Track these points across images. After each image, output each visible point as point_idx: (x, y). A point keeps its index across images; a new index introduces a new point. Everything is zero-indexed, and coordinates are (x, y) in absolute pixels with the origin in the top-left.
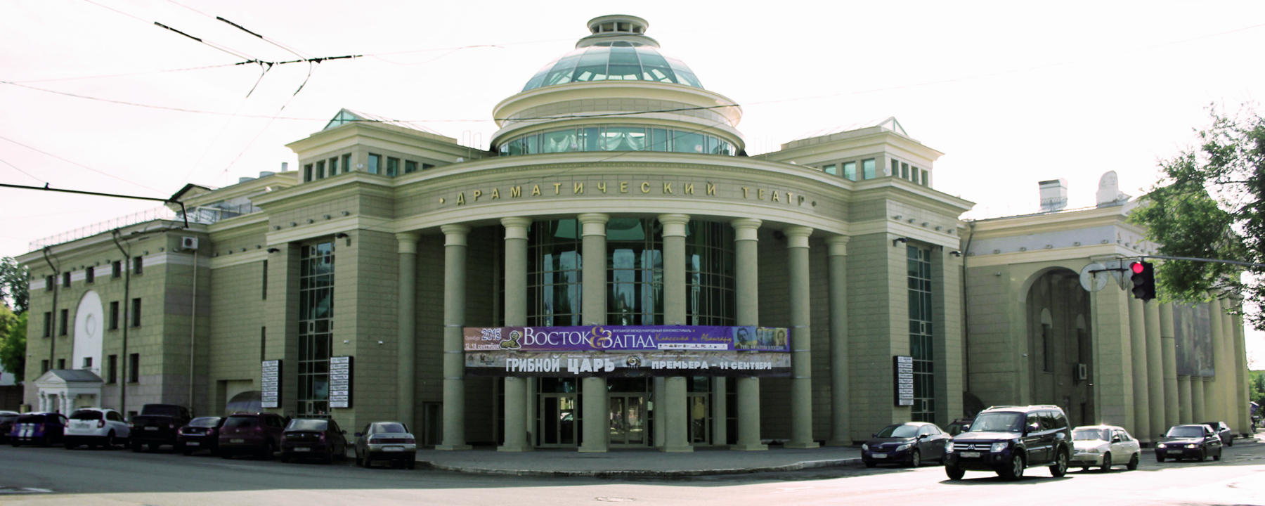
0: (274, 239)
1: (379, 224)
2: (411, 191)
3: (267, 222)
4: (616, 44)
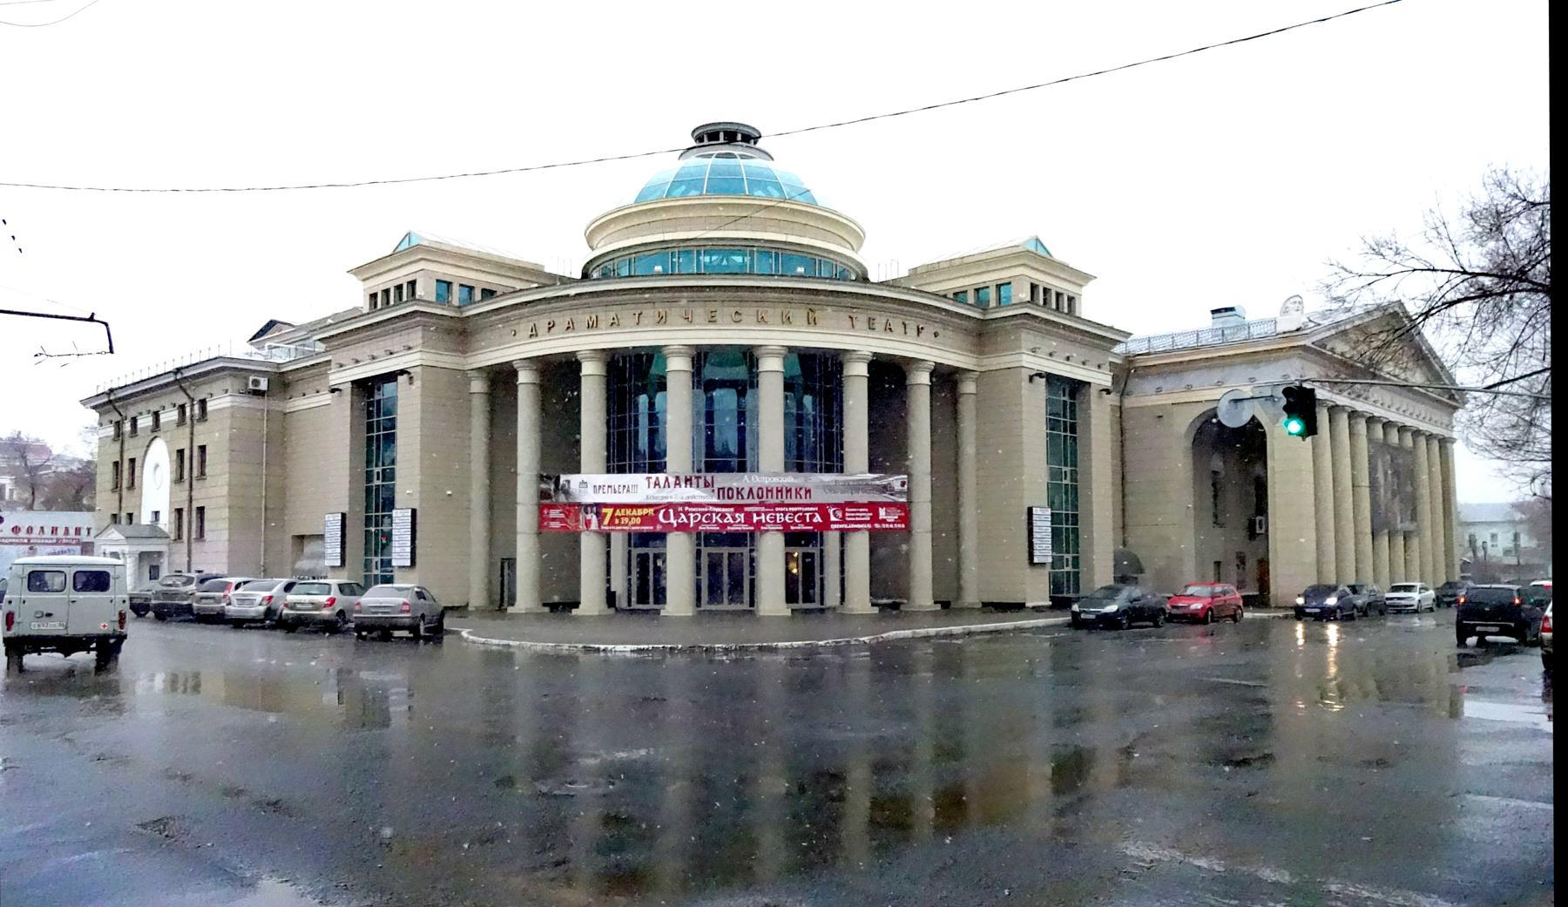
0: (336, 378)
1: (447, 360)
4: (718, 156)
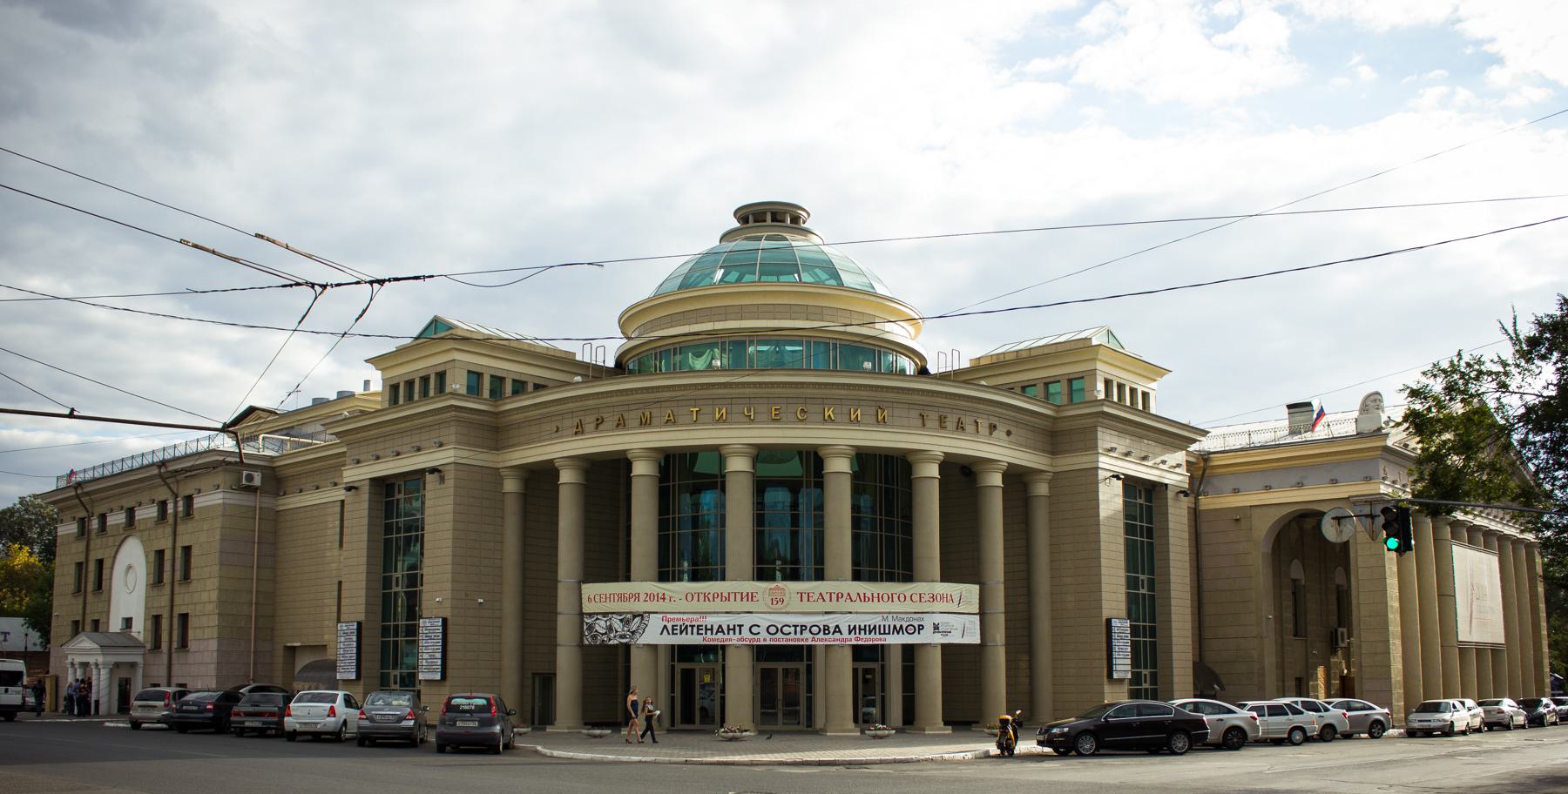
0: (351, 474)
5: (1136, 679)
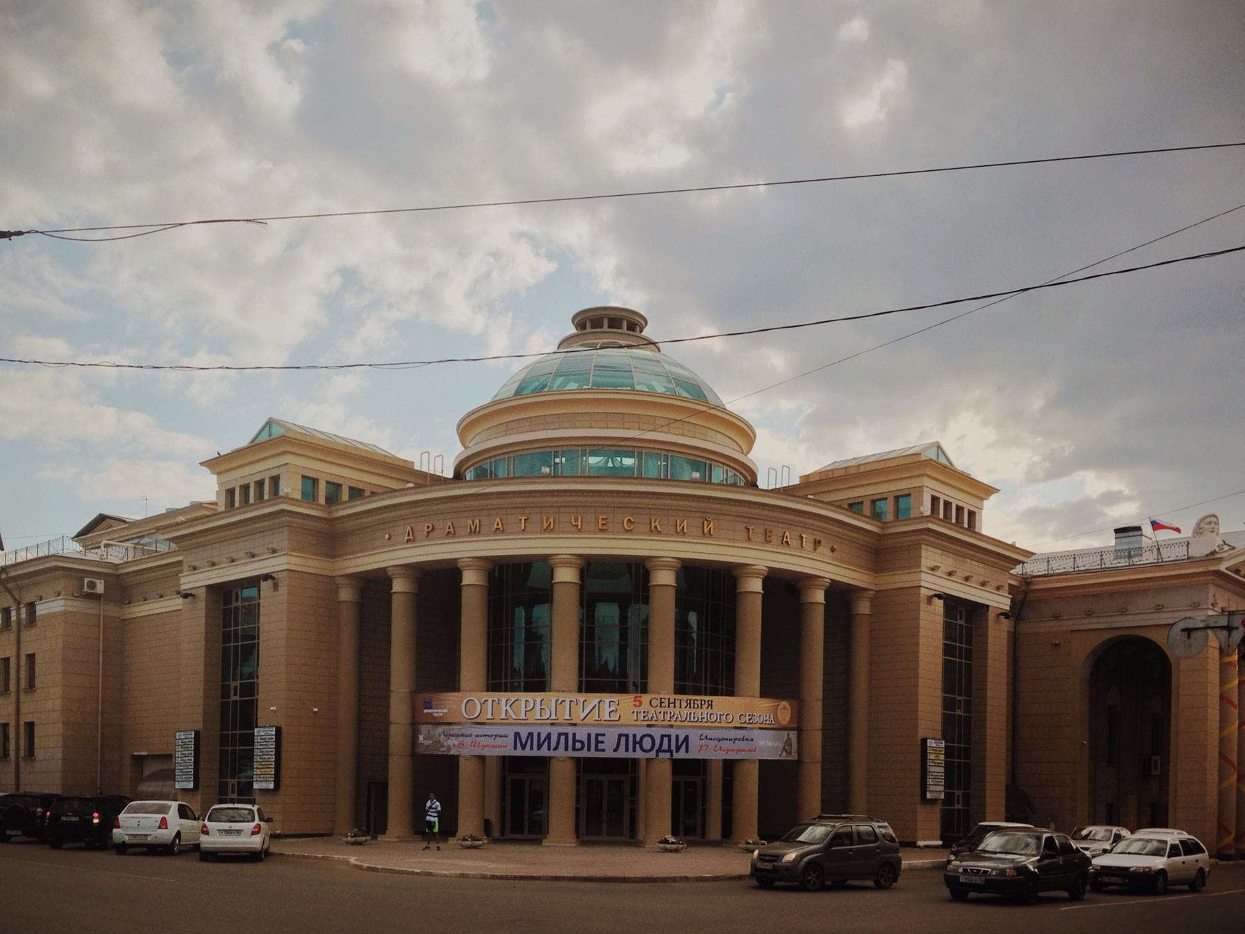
0: (189, 581)
1: (312, 564)
2: (351, 525)
3: (180, 562)
5: (949, 799)
